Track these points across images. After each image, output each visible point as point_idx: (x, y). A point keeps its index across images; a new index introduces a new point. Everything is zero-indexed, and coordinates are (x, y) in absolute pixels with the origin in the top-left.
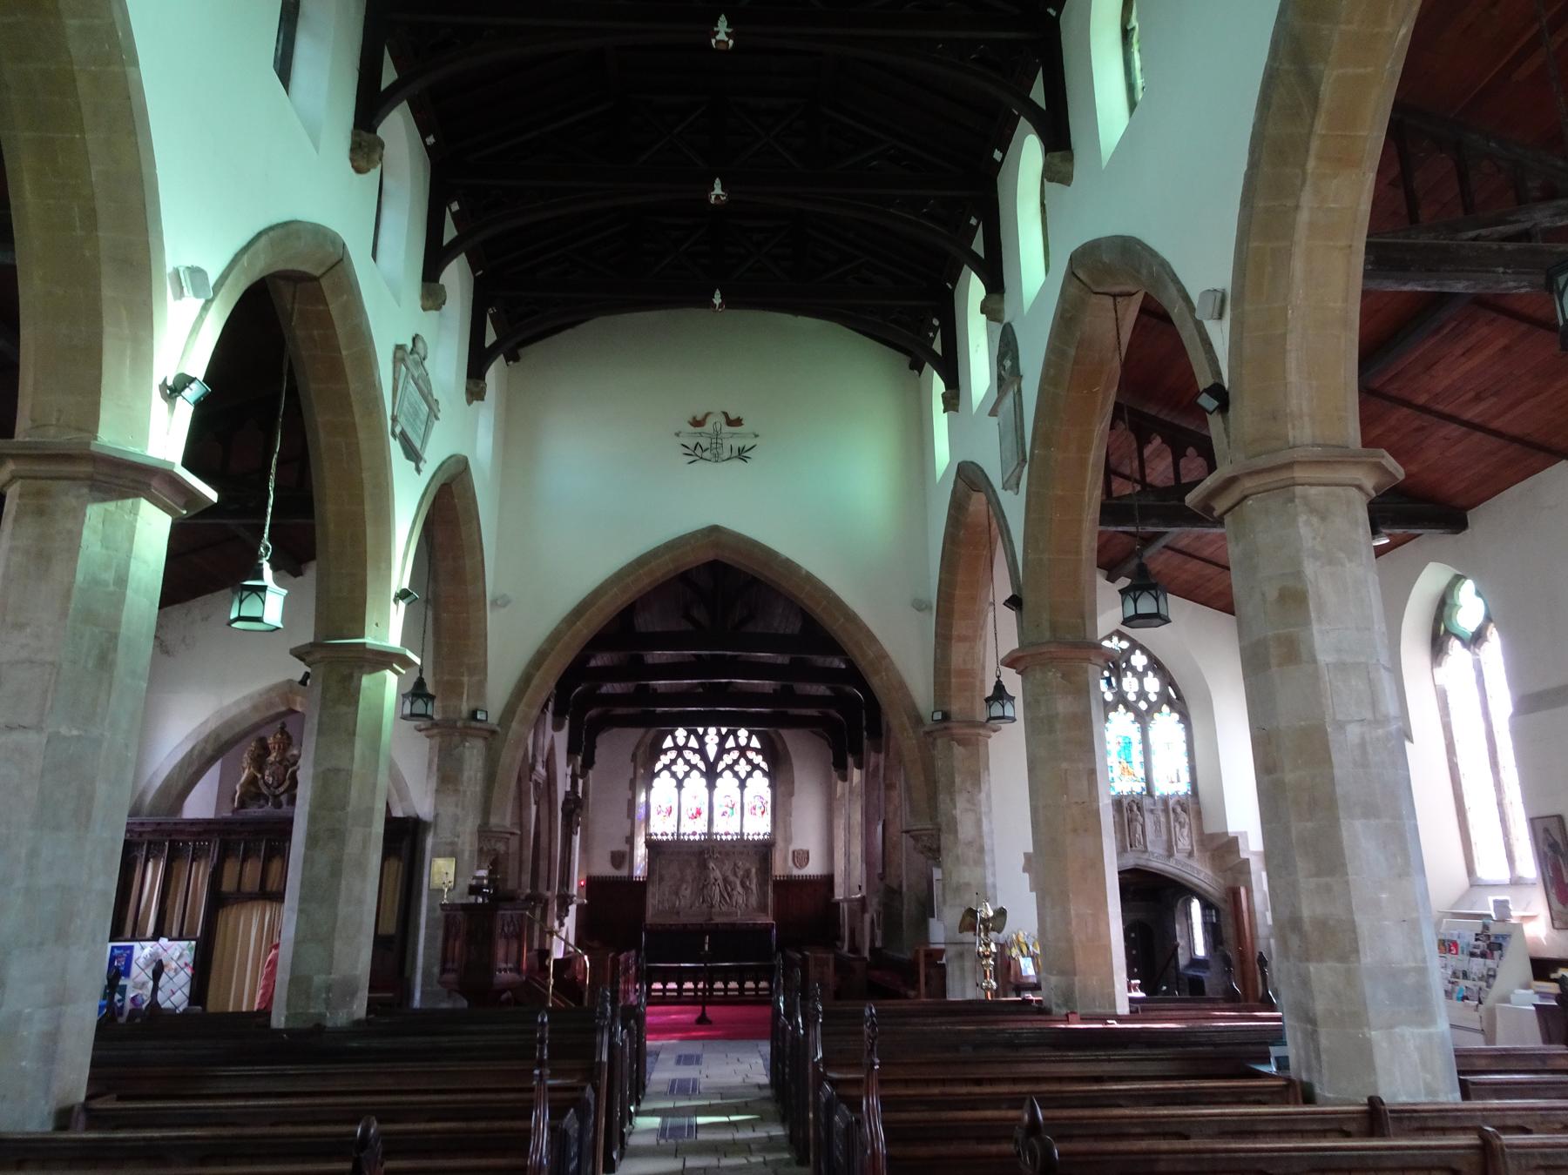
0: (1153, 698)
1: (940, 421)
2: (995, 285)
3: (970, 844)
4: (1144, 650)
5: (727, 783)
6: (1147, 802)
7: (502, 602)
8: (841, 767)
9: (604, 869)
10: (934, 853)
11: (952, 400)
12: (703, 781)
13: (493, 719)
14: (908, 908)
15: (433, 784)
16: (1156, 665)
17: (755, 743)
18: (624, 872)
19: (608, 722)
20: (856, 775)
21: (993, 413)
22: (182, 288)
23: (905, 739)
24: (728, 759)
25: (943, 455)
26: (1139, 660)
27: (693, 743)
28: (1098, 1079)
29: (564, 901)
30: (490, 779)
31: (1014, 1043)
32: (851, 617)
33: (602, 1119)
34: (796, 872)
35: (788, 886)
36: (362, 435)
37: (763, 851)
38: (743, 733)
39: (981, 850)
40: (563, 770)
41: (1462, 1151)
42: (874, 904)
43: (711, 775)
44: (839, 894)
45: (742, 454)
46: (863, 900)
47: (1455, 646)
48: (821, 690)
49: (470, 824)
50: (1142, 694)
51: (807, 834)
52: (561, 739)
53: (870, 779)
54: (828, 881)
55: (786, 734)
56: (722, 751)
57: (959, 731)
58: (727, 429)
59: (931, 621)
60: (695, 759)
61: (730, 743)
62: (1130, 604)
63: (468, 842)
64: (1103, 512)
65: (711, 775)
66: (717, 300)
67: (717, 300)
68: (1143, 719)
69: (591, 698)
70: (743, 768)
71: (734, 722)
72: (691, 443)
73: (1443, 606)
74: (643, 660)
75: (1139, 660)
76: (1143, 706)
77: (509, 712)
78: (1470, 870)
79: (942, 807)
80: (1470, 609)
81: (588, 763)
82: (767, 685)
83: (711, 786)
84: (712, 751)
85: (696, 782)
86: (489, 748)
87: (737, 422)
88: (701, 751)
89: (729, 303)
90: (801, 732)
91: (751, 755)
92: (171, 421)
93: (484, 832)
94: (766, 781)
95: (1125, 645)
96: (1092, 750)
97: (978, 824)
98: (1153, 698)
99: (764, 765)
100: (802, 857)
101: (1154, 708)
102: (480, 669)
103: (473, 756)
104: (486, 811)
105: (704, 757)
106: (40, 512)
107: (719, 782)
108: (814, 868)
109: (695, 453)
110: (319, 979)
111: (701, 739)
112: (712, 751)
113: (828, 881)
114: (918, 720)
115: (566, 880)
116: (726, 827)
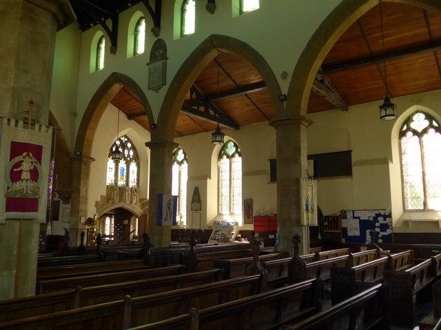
0: (131, 157)
4: (131, 142)
6: (127, 189)
16: (133, 148)
26: (129, 145)
28: (57, 278)
33: (303, 213)
39: (87, 199)
41: (268, 251)
47: (410, 134)
50: (129, 156)
57: (84, 159)
62: (214, 137)
67: (129, 5)
68: (128, 164)
73: (409, 120)
75: (129, 145)
76: (128, 159)
78: (218, 211)
80: (231, 149)
92: (420, 142)
95: (126, 140)
97: (87, 191)
98: (131, 157)
101: (131, 160)
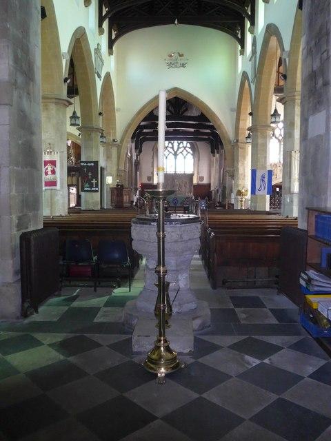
1: (240, 58)
2: (253, 24)
3: (242, 174)
5: (180, 156)
7: (118, 110)
8: (213, 152)
9: (145, 181)
10: (233, 176)
11: (242, 53)
12: (173, 157)
13: (119, 141)
14: (227, 191)
15: (105, 158)
17: (189, 145)
18: (151, 182)
19: (145, 140)
20: (217, 155)
21: (250, 60)
22: (72, 64)
23: (227, 147)
24: (180, 150)
25: (240, 69)
27: (170, 145)
29: (136, 189)
30: (119, 157)
31: (153, 158)
32: (213, 113)
34: (200, 183)
35: (198, 187)
36: (89, 75)
37: (191, 176)
38: (185, 142)
39: (245, 176)
40: (134, 154)
42: (220, 191)
43: (175, 154)
44: (212, 189)
45: (183, 66)
46: (217, 190)
48: (208, 131)
49: (115, 169)
51: (204, 174)
52: (133, 145)
53: (221, 156)
54: (209, 185)
55: (198, 143)
56: (179, 148)
58: (179, 58)
59: (235, 114)
60: (171, 150)
61: (181, 145)
63: (114, 173)
64: (275, 89)
65: (175, 154)
66: (176, 22)
67: (176, 22)
69: (141, 133)
70: (185, 153)
71: (182, 139)
72: (169, 62)
74: (205, 263)
77: (122, 141)
79: (235, 165)
81: (140, 151)
82: (192, 130)
83: (176, 158)
84: (176, 148)
85: (171, 157)
86: (118, 149)
87: (181, 55)
88: (173, 148)
89: (179, 22)
90: (202, 143)
91: (187, 149)
93: (118, 170)
94: (192, 157)
96: (266, 152)
97: (244, 170)
99: (191, 152)
100: (201, 178)
102: (114, 129)
103: (114, 151)
104: (118, 165)
105: (173, 150)
106: (47, 109)
107: (178, 157)
108: (205, 182)
109: (170, 65)
110: (91, 201)
111: (172, 144)
112: (176, 148)
113: (209, 185)
114: (230, 142)
115: (136, 184)
116: (180, 171)
